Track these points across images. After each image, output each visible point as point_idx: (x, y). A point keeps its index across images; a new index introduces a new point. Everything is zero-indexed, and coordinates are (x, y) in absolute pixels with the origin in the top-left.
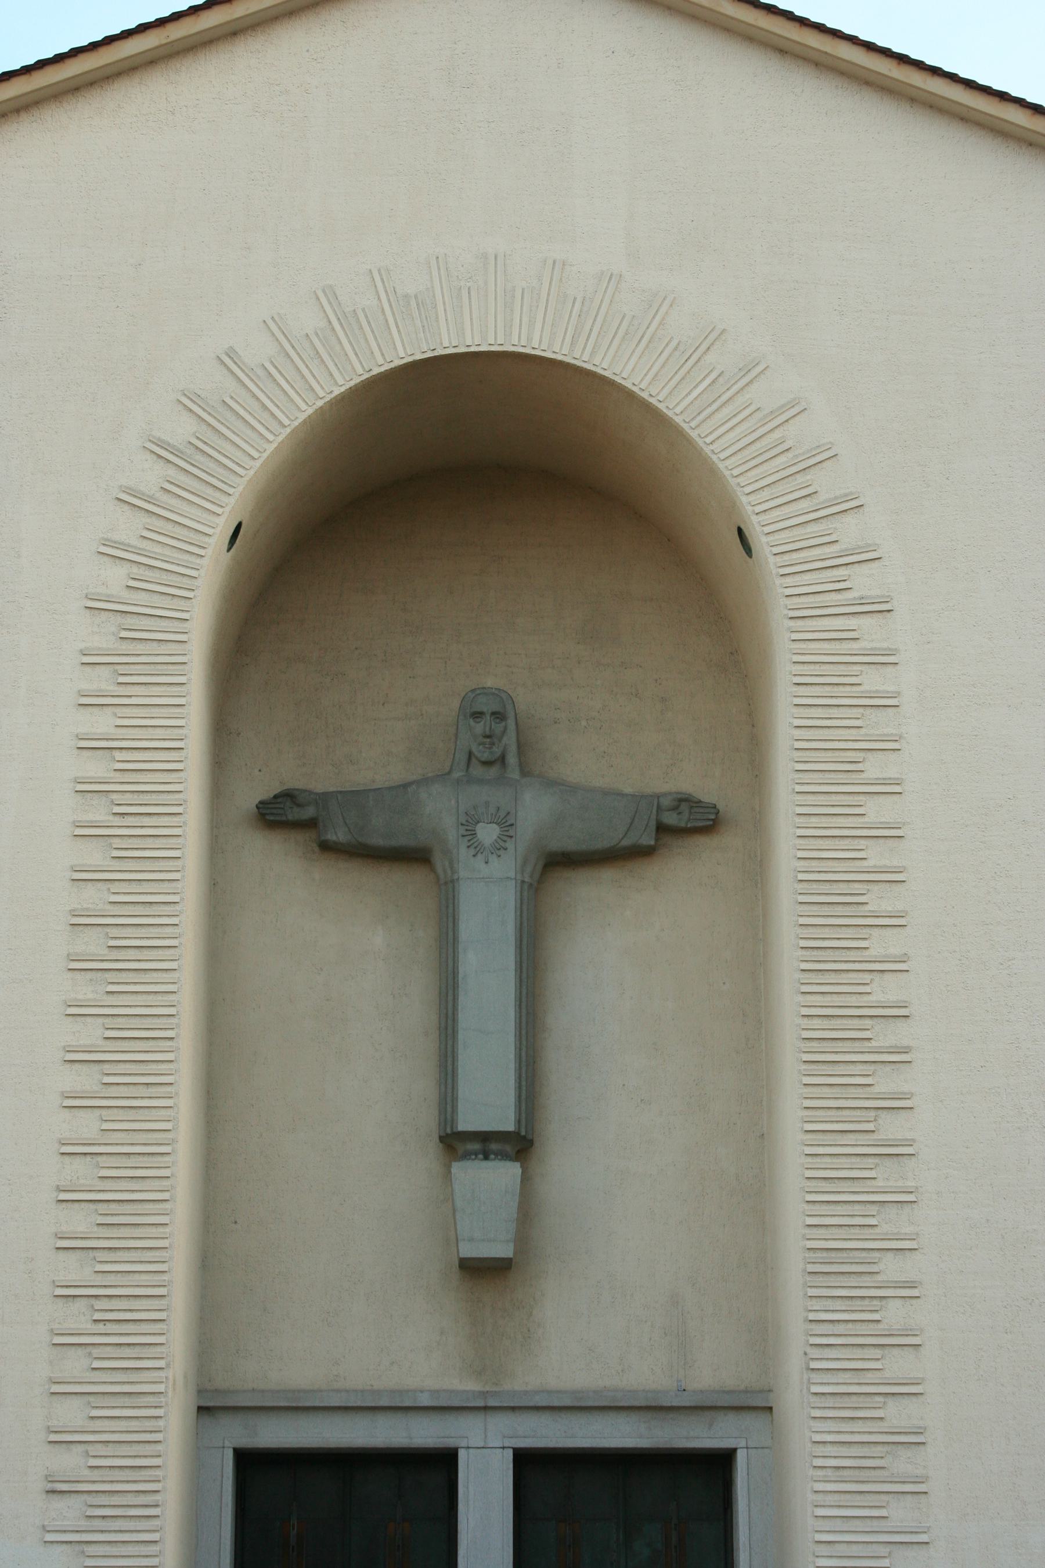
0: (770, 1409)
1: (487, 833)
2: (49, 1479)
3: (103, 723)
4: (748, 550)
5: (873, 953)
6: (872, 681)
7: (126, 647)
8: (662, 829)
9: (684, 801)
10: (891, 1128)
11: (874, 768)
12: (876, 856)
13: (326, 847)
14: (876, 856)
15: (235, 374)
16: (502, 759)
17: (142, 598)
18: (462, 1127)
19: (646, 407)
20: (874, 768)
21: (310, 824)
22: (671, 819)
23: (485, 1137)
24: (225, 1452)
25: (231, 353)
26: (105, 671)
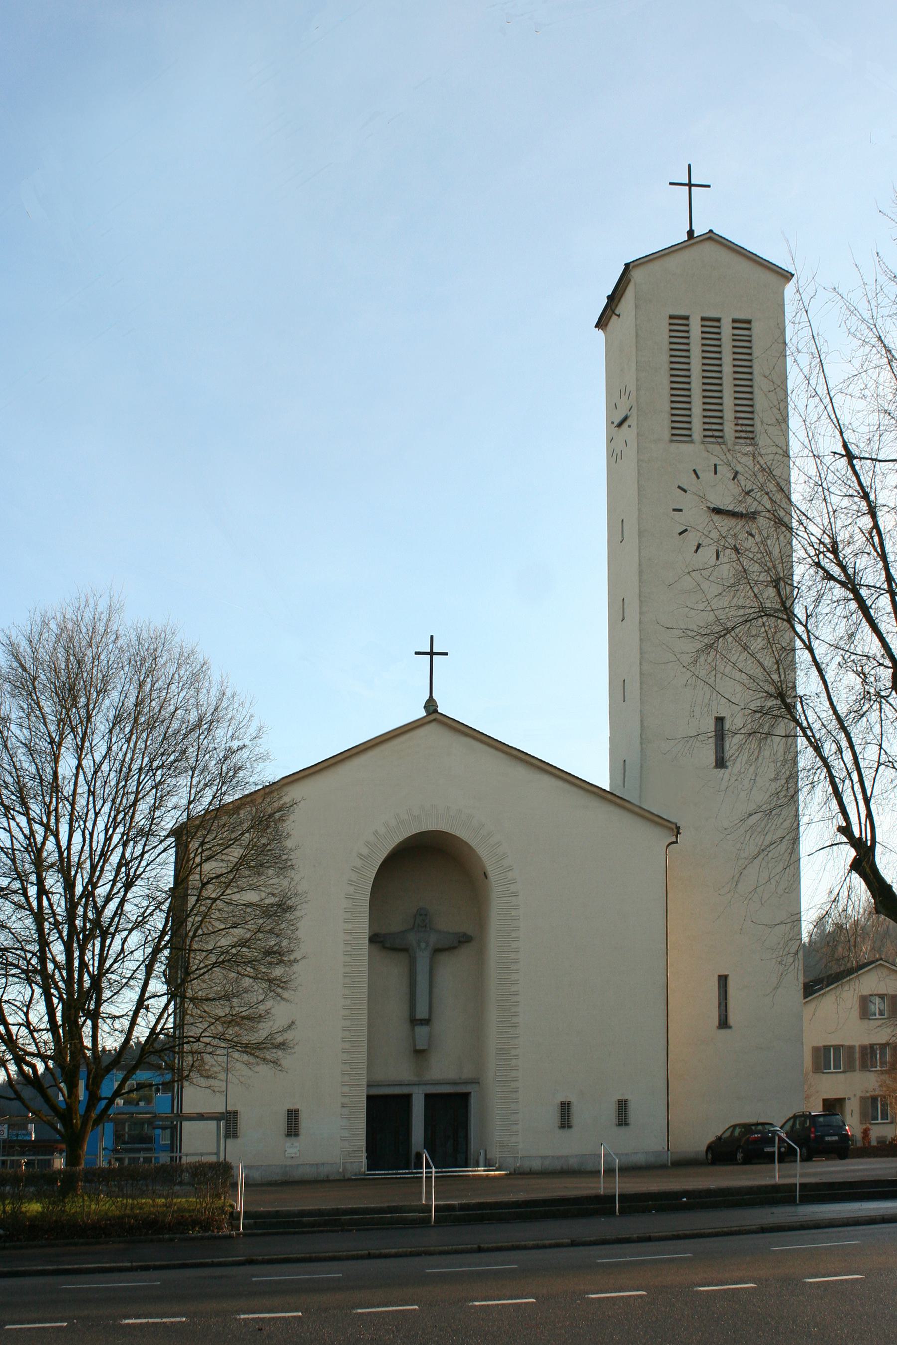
0: (479, 1083)
1: (423, 945)
2: (342, 1103)
3: (350, 926)
4: (487, 878)
5: (513, 979)
6: (514, 913)
7: (354, 907)
8: (460, 942)
9: (465, 934)
10: (515, 1020)
11: (514, 934)
12: (513, 955)
13: (384, 948)
14: (513, 955)
15: (799, 1230)
16: (425, 926)
17: (357, 894)
18: (417, 1018)
19: (467, 844)
20: (514, 934)
21: (381, 942)
22: (462, 939)
23: (421, 1020)
24: (48, 1086)
25: (376, 831)
26: (350, 913)
